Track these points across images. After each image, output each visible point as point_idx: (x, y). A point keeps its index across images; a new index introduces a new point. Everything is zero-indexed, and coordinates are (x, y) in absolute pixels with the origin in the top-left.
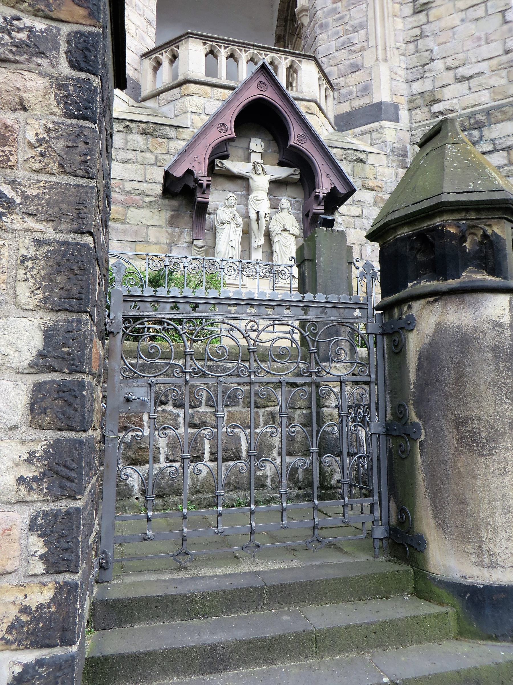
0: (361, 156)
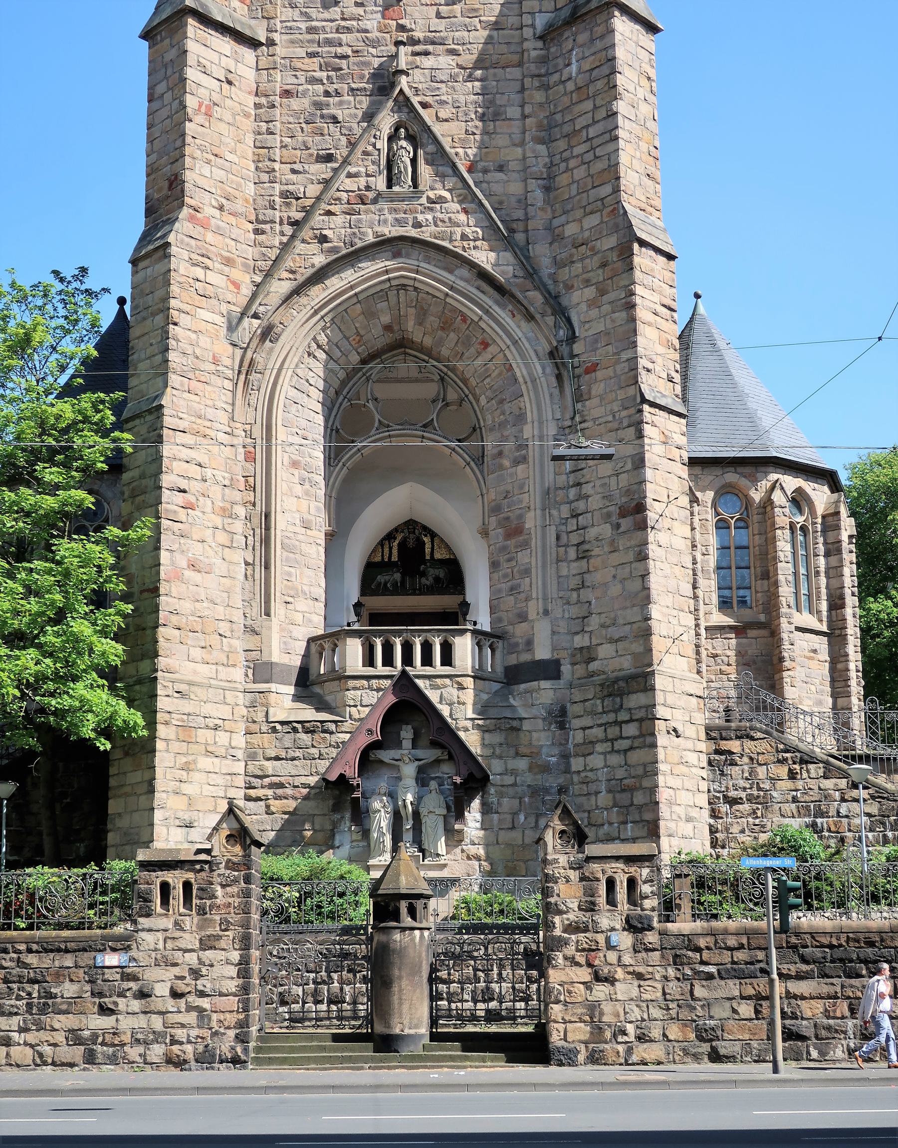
0: (515, 724)
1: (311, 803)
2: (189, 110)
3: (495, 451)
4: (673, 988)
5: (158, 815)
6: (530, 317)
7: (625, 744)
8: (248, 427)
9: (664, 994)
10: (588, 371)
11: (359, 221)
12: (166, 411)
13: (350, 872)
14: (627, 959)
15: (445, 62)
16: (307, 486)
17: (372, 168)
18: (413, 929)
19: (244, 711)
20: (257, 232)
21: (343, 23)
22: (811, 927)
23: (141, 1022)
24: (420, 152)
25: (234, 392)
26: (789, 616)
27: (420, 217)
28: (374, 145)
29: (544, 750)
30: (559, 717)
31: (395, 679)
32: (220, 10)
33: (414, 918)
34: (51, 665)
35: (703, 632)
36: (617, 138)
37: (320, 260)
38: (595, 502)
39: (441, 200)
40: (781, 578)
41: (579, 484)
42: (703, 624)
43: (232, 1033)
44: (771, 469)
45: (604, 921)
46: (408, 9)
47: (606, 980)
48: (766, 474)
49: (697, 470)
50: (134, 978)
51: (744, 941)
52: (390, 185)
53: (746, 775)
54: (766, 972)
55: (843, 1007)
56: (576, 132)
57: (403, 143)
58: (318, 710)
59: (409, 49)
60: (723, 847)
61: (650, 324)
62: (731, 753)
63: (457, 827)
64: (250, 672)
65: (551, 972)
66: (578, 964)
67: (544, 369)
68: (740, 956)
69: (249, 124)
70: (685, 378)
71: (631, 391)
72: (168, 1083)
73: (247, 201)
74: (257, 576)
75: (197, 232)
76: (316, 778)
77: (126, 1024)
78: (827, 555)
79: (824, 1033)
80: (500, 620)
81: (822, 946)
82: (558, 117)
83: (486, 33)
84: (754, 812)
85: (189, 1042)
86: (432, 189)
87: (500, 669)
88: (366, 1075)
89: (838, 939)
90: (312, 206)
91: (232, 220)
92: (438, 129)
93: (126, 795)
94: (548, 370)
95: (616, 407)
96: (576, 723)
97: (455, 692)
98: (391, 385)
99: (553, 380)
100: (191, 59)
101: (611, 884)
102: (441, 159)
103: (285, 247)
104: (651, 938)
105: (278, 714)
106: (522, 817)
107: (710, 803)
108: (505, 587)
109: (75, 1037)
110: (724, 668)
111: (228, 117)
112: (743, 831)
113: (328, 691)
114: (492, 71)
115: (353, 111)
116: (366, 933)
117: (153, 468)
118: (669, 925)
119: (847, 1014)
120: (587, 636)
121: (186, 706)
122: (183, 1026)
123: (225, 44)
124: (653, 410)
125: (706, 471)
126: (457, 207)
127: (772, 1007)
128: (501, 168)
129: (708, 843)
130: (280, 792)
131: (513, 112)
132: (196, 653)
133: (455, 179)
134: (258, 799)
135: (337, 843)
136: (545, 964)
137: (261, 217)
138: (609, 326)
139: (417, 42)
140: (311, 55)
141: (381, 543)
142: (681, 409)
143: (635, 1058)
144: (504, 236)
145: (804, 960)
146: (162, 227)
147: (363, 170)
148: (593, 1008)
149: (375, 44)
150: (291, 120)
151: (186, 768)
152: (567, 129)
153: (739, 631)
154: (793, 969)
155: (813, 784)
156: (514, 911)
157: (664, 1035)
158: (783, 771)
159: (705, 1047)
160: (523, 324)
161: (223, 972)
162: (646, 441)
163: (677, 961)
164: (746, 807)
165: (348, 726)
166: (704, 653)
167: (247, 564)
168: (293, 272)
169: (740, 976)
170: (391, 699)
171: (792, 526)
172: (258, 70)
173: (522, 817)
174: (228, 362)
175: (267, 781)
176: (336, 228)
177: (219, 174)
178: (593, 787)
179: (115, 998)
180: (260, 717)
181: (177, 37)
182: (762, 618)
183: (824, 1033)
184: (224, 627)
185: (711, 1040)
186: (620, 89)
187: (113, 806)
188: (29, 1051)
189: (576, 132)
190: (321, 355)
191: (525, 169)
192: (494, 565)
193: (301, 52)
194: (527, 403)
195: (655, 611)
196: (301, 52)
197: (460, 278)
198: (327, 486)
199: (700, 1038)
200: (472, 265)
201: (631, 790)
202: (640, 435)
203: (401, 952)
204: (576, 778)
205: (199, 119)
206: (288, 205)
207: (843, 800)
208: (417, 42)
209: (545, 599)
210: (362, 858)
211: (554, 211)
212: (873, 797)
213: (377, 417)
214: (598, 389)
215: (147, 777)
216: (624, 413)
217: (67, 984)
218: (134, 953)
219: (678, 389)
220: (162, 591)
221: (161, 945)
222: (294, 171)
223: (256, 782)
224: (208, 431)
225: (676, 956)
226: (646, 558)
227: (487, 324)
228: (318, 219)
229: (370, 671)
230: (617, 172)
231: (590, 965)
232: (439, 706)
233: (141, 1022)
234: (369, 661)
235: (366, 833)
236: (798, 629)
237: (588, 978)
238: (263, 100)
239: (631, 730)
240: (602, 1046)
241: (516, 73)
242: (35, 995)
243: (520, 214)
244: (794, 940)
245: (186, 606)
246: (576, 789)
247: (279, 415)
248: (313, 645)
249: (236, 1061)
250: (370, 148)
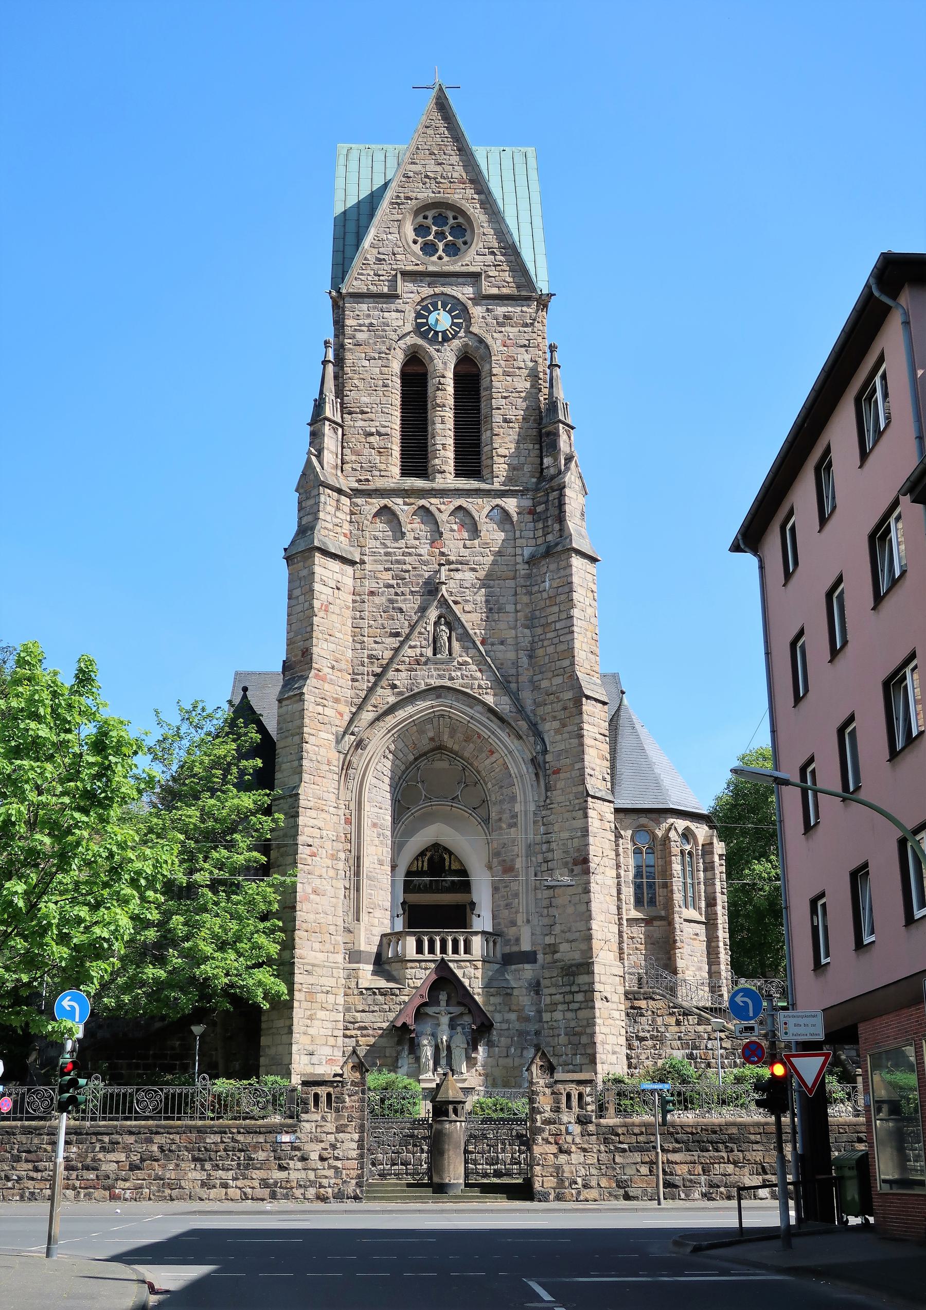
0: (509, 991)
1: (384, 1040)
2: (315, 609)
3: (497, 818)
4: (603, 1156)
5: (295, 1048)
6: (519, 737)
7: (576, 1006)
8: (347, 803)
9: (598, 1160)
10: (555, 773)
11: (416, 675)
12: (301, 797)
13: (410, 1084)
14: (578, 1140)
15: (469, 576)
16: (381, 838)
17: (424, 643)
18: (456, 1121)
19: (343, 981)
20: (353, 680)
21: (407, 550)
22: (681, 1122)
23: (302, 1175)
24: (454, 634)
25: (339, 782)
26: (680, 913)
27: (453, 674)
28: (425, 628)
29: (527, 1008)
30: (536, 987)
31: (437, 963)
32: (334, 544)
33: (456, 1115)
34: (244, 962)
35: (625, 922)
36: (573, 632)
37: (392, 700)
38: (558, 855)
39: (465, 663)
40: (675, 888)
41: (549, 842)
42: (625, 917)
43: (354, 1182)
44: (669, 815)
45: (565, 1118)
46: (446, 542)
47: (566, 1152)
48: (666, 819)
49: (621, 816)
50: (299, 1149)
51: (644, 1130)
52: (435, 654)
53: (650, 1022)
54: (655, 1148)
55: (699, 1169)
56: (548, 624)
57: (443, 627)
58: (388, 981)
59: (447, 567)
60: (636, 1068)
61: (592, 747)
62: (640, 1008)
63: (473, 1055)
64: (347, 956)
65: (535, 1147)
66: (550, 1143)
67: (527, 769)
68: (641, 1138)
69: (349, 613)
70: (613, 775)
71: (581, 788)
73: (347, 661)
74: (352, 896)
75: (319, 684)
76: (388, 1024)
77: (294, 1175)
78: (705, 870)
79: (688, 1184)
80: (499, 924)
81: (688, 1133)
82: (537, 613)
83: (492, 558)
84: (655, 1046)
85: (330, 1187)
86: (461, 656)
87: (499, 955)
88: (430, 1206)
89: (696, 1129)
90: (387, 664)
91: (339, 674)
92: (463, 618)
93: (273, 1034)
94: (530, 770)
95: (571, 797)
96: (546, 991)
97: (472, 971)
98: (431, 774)
99: (534, 776)
100: (317, 578)
101: (569, 1096)
102: (465, 637)
103: (371, 690)
104: (591, 1128)
105: (364, 984)
106: (513, 1050)
107: (627, 1040)
108: (502, 903)
109: (264, 1183)
110: (639, 946)
111: (337, 611)
112: (648, 1058)
113: (394, 968)
114: (497, 582)
115: (413, 605)
116: (428, 1123)
117: (292, 831)
118: (601, 1120)
119: (701, 1172)
120: (553, 937)
121: (311, 980)
122: (326, 1177)
123: (335, 565)
124: (593, 800)
125: (627, 816)
126: (474, 667)
127: (658, 1168)
128: (502, 643)
129: (625, 1067)
130: (365, 1032)
131: (510, 608)
132: (317, 946)
133: (474, 651)
134: (352, 1037)
135: (400, 1065)
136: (531, 1142)
137: (356, 671)
138: (568, 747)
139: (451, 563)
140: (387, 570)
141: (417, 859)
142: (610, 798)
143: (582, 1198)
144: (503, 684)
145: (677, 1141)
146: (298, 680)
147: (418, 643)
148: (558, 1168)
149: (426, 563)
150: (374, 610)
151: (311, 1018)
152: (543, 621)
153: (648, 922)
154: (671, 1146)
155: (691, 1028)
156: (509, 1109)
157: (598, 1184)
158: (672, 1020)
159: (622, 1192)
160: (516, 741)
161: (349, 1144)
162: (590, 820)
163: (606, 1141)
164: (650, 1043)
165: (406, 991)
166: (625, 936)
167: (346, 888)
168: (375, 707)
169: (641, 1150)
170: (434, 977)
171: (682, 852)
172: (354, 579)
173: (513, 1050)
174: (336, 763)
175: (357, 1025)
176: (401, 679)
177: (332, 647)
178: (556, 1032)
179: (287, 1161)
180: (353, 985)
181: (309, 563)
182: (663, 913)
183: (688, 1184)
184: (332, 929)
185: (624, 1188)
186: (575, 602)
187: (264, 1041)
188: (238, 1191)
189: (548, 624)
190: (390, 756)
191: (517, 644)
192: (496, 889)
193: (381, 568)
194: (517, 790)
195: (594, 925)
196: (381, 568)
197: (477, 712)
198: (392, 836)
199: (619, 1186)
200: (485, 704)
201: (579, 1034)
202: (586, 816)
203: (449, 1135)
204: (546, 1026)
205: (322, 614)
206: (372, 663)
207: (709, 1039)
208: (451, 563)
209: (527, 913)
210: (415, 1075)
211: (534, 671)
212: (728, 1037)
213: (424, 793)
214: (560, 784)
215: (287, 1023)
216: (577, 801)
217: (260, 1152)
218: (298, 1134)
219: (609, 784)
220: (298, 908)
221: (314, 1130)
222: (376, 642)
223: (350, 1026)
224: (324, 807)
225: (605, 1139)
226: (589, 892)
227: (493, 740)
228: (391, 674)
229: (420, 957)
230: (573, 652)
231: (557, 1143)
232: (462, 979)
233: (302, 1175)
234: (420, 950)
235: (418, 1059)
236: (685, 920)
237: (556, 1151)
238: (358, 598)
239: (579, 997)
240: (563, 1191)
241: (511, 583)
242: (242, 1158)
243: (513, 671)
244: (671, 1130)
245: (311, 917)
246: (545, 1032)
247: (366, 795)
248: (384, 939)
249: (356, 1198)
250: (423, 630)
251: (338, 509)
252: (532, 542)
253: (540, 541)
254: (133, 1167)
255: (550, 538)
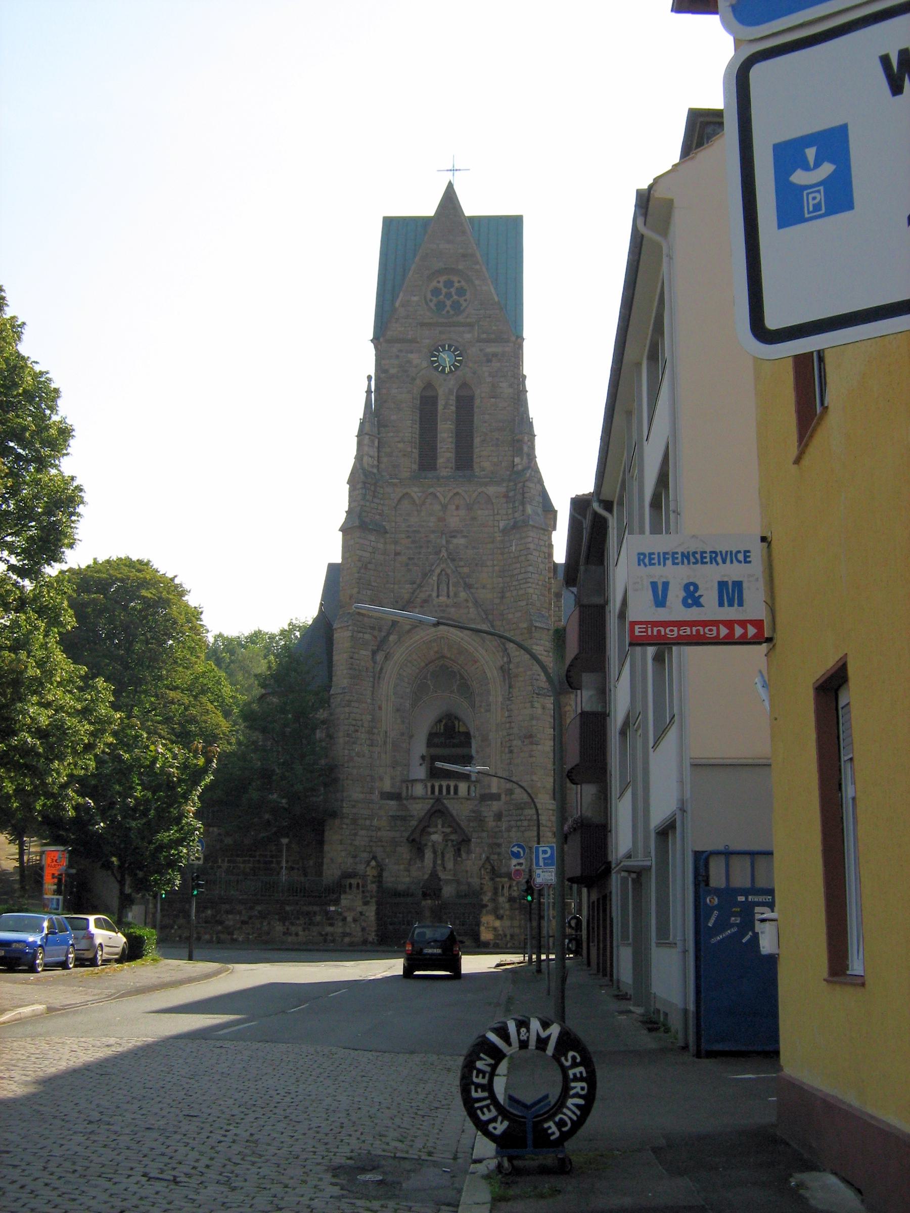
72: (167, 977)
87: (478, 795)
128: (484, 587)
141: (436, 724)
251: (374, 497)
252: (505, 517)
253: (511, 516)
254: (244, 923)
255: (516, 515)
